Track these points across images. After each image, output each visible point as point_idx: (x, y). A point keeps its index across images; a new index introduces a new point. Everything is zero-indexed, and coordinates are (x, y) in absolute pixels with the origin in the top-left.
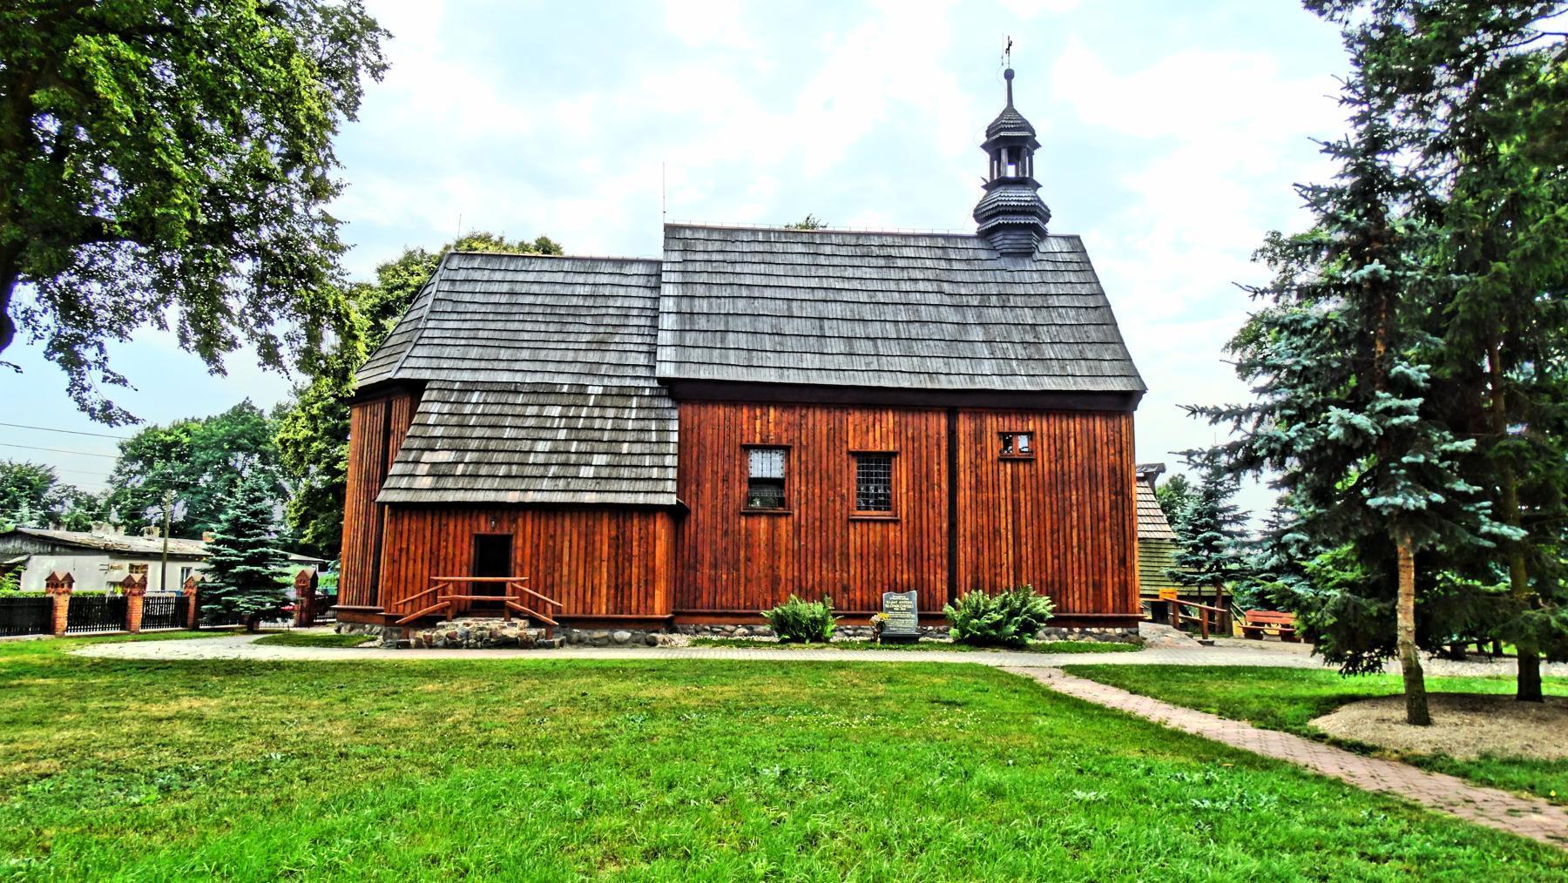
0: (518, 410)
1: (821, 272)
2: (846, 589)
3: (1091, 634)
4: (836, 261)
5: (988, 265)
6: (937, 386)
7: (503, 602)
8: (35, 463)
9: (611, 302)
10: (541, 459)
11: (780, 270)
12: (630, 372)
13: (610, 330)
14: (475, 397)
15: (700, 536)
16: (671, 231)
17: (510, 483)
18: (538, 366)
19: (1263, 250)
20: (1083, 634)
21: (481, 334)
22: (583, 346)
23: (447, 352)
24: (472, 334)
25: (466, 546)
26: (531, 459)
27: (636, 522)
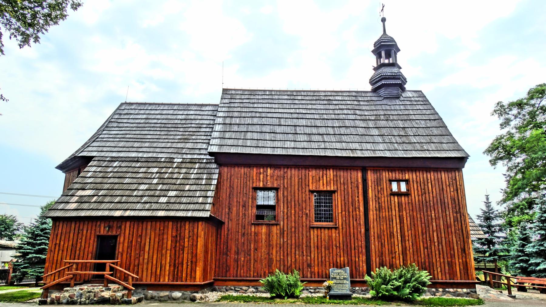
0: (136, 170)
1: (296, 106)
2: (309, 266)
3: (449, 292)
5: (378, 103)
6: (356, 155)
7: (103, 275)
8: (8, 215)
9: (193, 122)
10: (140, 193)
11: (277, 106)
12: (197, 152)
13: (191, 133)
14: (116, 164)
15: (230, 236)
16: (225, 91)
17: (119, 206)
18: (152, 150)
19: (495, 111)
21: (127, 136)
22: (176, 141)
23: (108, 144)
24: (123, 136)
26: (135, 193)
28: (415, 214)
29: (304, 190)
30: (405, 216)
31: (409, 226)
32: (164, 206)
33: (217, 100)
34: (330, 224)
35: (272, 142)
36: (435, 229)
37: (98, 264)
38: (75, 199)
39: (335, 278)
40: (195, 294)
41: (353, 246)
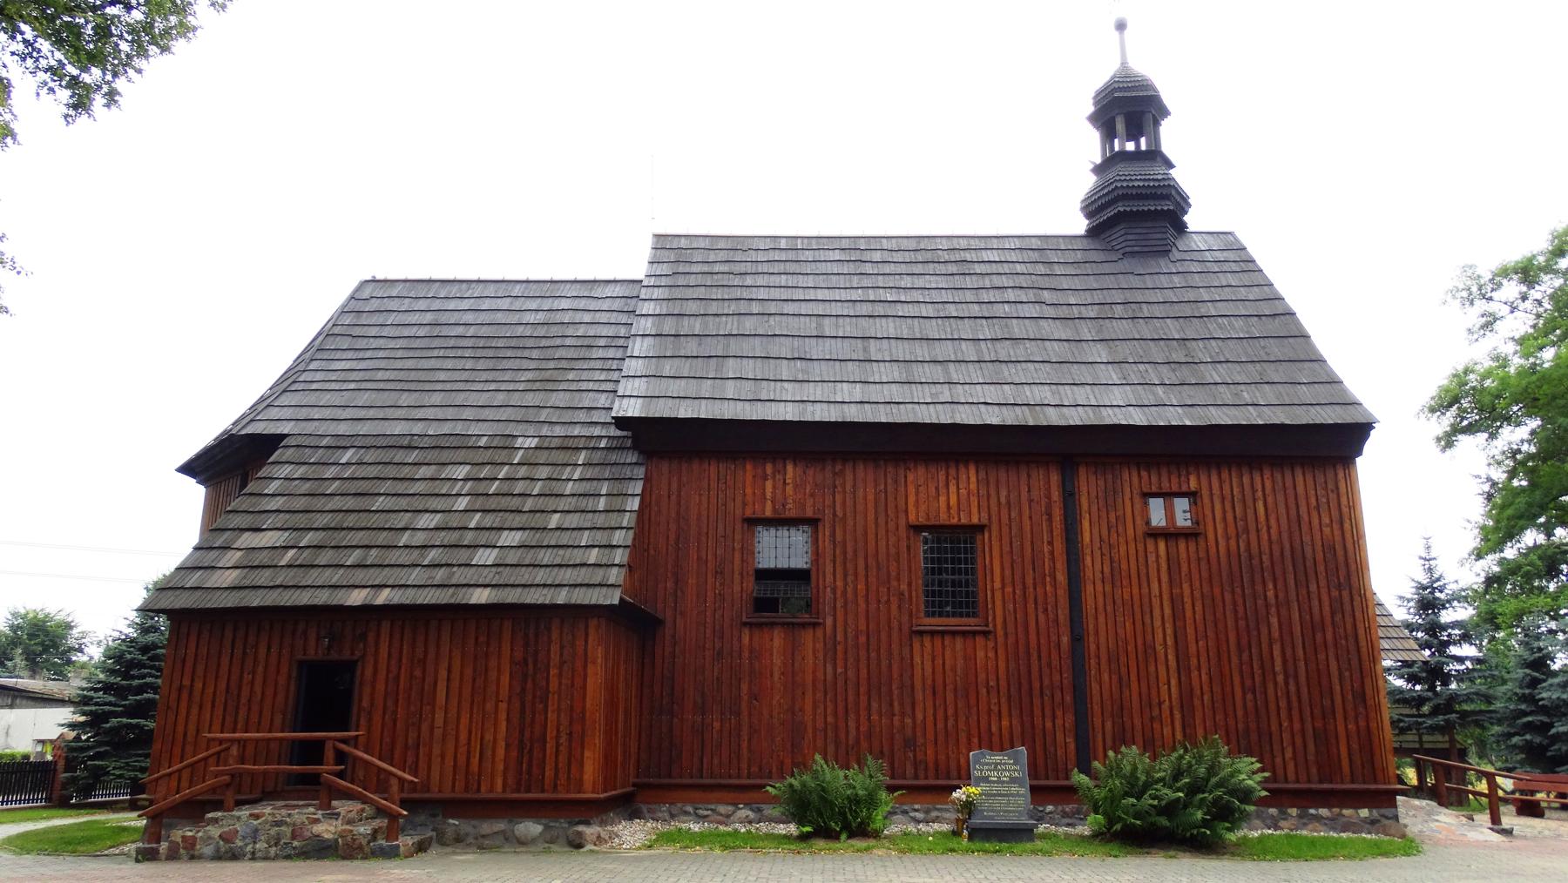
1: (866, 282)
2: (910, 743)
3: (1318, 818)
4: (887, 269)
9: (570, 331)
10: (420, 538)
11: (810, 281)
13: (564, 364)
17: (360, 576)
18: (450, 413)
20: (1305, 821)
22: (521, 386)
23: (326, 399)
25: (282, 681)
26: (405, 539)
27: (555, 635)
28: (1217, 591)
29: (891, 525)
30: (1187, 600)
31: (1201, 628)
32: (489, 576)
33: (637, 267)
34: (970, 623)
35: (797, 385)
36: (1276, 634)
37: (302, 742)
38: (233, 557)
39: (986, 779)
40: (581, 828)
41: (1036, 685)
